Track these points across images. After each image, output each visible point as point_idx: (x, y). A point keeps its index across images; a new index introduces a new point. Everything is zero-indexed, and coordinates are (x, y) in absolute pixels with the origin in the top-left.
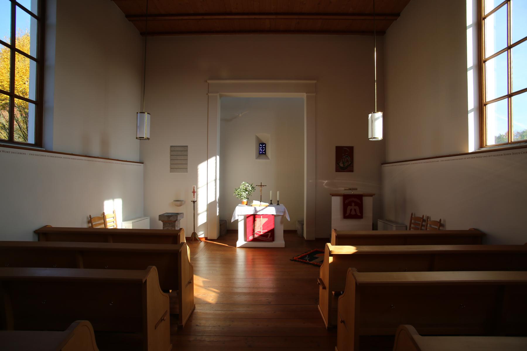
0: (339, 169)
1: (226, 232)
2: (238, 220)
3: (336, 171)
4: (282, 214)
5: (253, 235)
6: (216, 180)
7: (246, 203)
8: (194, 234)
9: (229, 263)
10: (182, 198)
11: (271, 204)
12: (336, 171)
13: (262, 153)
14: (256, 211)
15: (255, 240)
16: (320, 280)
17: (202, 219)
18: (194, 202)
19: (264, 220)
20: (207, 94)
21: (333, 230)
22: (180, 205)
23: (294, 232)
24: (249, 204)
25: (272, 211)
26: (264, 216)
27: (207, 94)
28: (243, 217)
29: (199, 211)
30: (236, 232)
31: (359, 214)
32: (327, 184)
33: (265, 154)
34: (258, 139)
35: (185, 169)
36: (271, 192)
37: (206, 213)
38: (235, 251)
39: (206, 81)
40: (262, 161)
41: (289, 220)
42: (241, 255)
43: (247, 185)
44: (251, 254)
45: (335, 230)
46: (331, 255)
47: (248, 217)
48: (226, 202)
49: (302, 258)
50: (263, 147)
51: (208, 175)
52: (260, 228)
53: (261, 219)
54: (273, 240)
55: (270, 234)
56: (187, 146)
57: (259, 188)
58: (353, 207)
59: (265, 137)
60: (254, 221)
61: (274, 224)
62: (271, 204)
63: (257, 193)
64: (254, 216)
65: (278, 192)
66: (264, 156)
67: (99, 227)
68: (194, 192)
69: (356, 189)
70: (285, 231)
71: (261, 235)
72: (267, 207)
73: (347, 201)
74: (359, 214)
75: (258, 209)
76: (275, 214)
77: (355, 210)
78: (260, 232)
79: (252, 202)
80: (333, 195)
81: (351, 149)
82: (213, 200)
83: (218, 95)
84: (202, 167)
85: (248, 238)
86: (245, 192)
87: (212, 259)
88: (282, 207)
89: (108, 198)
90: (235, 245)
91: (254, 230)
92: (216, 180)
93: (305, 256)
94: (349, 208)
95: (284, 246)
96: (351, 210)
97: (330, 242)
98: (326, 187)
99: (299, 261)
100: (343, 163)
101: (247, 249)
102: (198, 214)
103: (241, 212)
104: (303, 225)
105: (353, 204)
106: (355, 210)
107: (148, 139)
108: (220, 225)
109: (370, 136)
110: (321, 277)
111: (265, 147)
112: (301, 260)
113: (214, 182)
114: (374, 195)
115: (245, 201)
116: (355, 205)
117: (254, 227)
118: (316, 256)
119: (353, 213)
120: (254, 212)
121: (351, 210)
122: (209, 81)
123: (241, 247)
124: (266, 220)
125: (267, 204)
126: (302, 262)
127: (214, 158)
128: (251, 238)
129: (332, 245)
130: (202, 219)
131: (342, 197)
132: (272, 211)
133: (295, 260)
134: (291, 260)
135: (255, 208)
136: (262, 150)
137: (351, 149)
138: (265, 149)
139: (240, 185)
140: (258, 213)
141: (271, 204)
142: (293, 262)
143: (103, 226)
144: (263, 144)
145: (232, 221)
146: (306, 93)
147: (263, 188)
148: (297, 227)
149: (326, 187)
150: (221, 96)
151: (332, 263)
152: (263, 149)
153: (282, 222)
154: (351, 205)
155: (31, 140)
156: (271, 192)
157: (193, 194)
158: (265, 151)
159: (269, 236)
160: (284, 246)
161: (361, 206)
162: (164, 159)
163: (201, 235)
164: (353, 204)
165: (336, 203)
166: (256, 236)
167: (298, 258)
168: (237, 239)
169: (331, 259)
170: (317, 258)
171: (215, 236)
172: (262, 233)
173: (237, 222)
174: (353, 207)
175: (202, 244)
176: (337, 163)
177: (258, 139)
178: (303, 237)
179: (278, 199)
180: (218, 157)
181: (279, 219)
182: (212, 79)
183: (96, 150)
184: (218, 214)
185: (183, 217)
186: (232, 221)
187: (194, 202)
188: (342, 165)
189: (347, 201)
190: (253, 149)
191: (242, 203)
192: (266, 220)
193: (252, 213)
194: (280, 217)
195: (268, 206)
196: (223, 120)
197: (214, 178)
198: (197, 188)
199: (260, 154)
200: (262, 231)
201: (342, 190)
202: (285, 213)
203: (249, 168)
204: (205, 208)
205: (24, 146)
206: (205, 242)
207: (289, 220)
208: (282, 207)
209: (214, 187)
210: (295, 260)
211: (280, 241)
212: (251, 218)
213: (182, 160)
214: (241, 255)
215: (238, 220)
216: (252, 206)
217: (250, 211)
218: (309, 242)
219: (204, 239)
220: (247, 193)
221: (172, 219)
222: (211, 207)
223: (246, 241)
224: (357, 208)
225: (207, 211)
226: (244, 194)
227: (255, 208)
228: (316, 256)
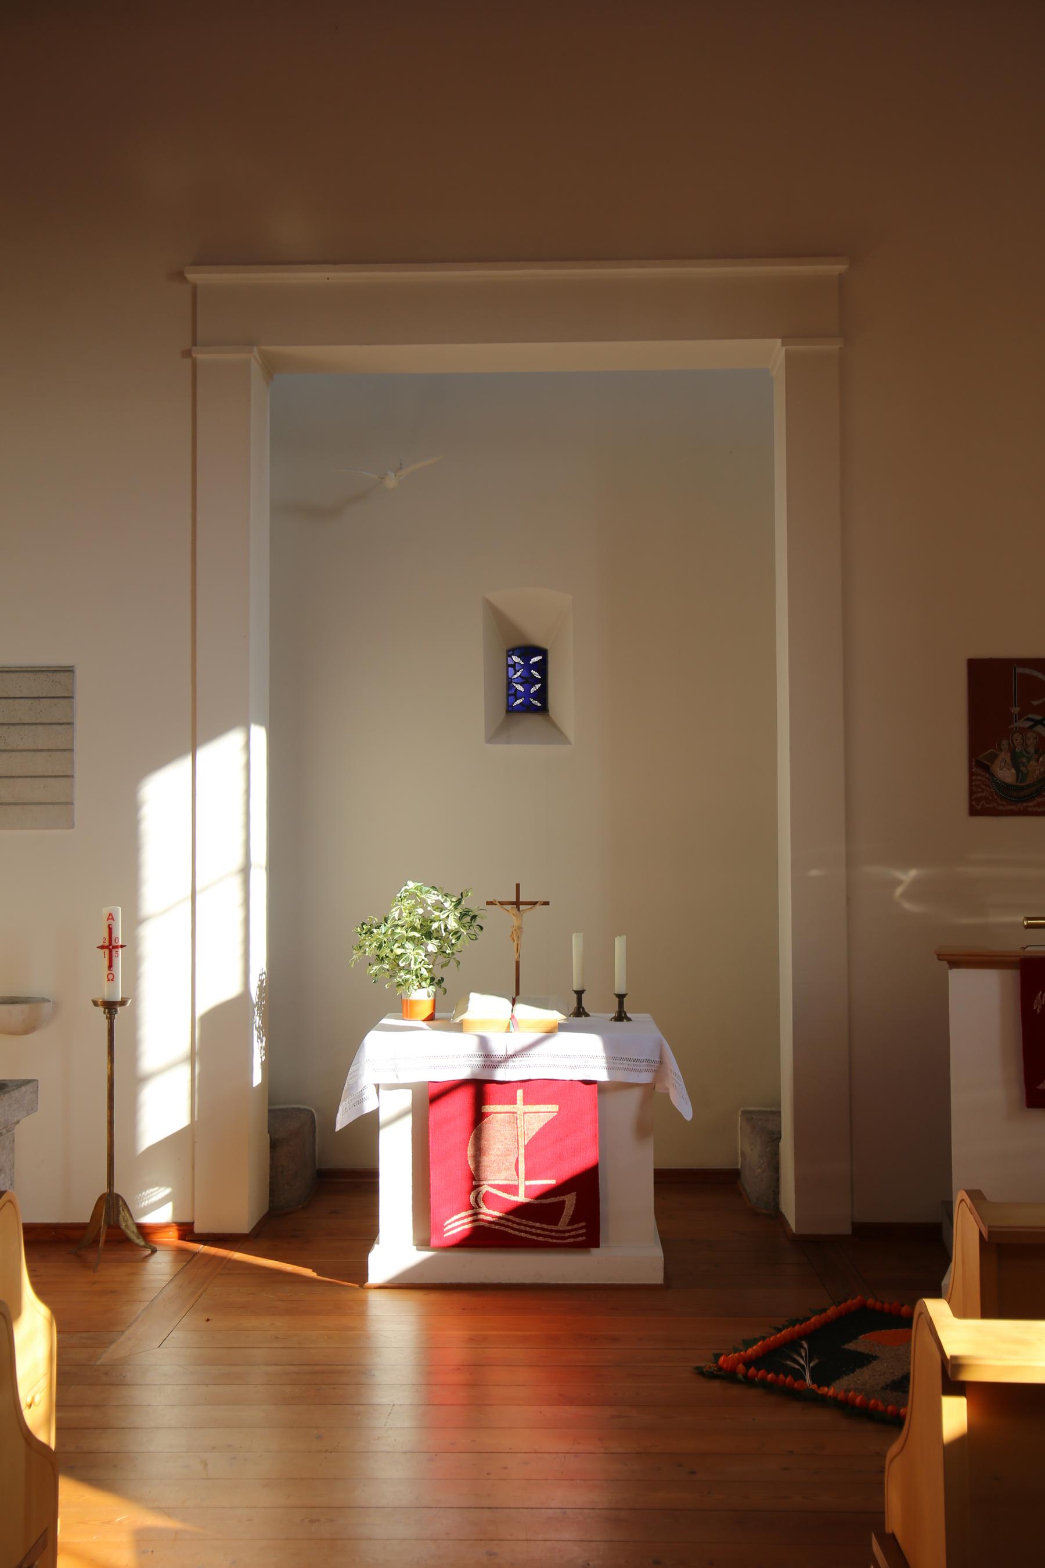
1: (311, 1187)
2: (375, 1114)
3: (973, 812)
4: (645, 1078)
5: (474, 1209)
6: (246, 871)
7: (427, 1012)
8: (111, 1204)
9: (324, 1389)
10: (37, 984)
11: (578, 1012)
12: (973, 812)
13: (527, 708)
14: (490, 1061)
15: (481, 1238)
16: (890, 1543)
17: (164, 1108)
18: (111, 1007)
19: (537, 1117)
20: (187, 353)
21: (960, 1196)
22: (28, 1029)
23: (723, 1181)
24: (444, 1015)
25: (582, 1056)
26: (538, 1090)
27: (187, 353)
28: (405, 1099)
29: (150, 1058)
30: (365, 1182)
32: (916, 891)
33: (544, 709)
34: (498, 620)
35: (60, 809)
36: (577, 942)
37: (185, 1071)
38: (360, 1311)
39: (180, 276)
40: (526, 753)
41: (687, 1112)
42: (394, 1333)
43: (432, 898)
44: (456, 1333)
45: (976, 1196)
46: (954, 1386)
47: (434, 1096)
48: (306, 1005)
49: (773, 1357)
50: (528, 667)
51: (199, 842)
52: (512, 1166)
53: (520, 1107)
54: (591, 1240)
55: (570, 1200)
56: (69, 670)
57: (508, 917)
59: (545, 610)
60: (478, 1118)
61: (600, 1137)
62: (580, 1012)
63: (494, 947)
64: (480, 1091)
65: (620, 944)
66: (533, 721)
68: (110, 947)
70: (666, 1180)
71: (520, 1211)
72: (551, 1032)
75: (500, 1047)
76: (601, 1075)
78: (512, 1189)
79: (461, 1003)
80: (958, 961)
82: (232, 990)
83: (253, 358)
84: (162, 793)
85: (440, 1229)
86: (417, 943)
87: (219, 1369)
88: (644, 1030)
90: (360, 1274)
91: (475, 1180)
92: (246, 871)
93: (792, 1345)
95: (657, 1277)
97: (937, 1294)
98: (907, 906)
99: (749, 1382)
100: (1016, 763)
101: (434, 1297)
102: (138, 1081)
103: (393, 1068)
104: (775, 1138)
108: (274, 1145)
110: (894, 1523)
112: (766, 1373)
113: (237, 881)
115: (422, 996)
117: (479, 1152)
118: (860, 1344)
120: (490, 1064)
122: (197, 277)
123: (398, 1285)
124: (547, 1111)
125: (556, 1016)
126: (764, 1385)
127: (234, 739)
128: (457, 1225)
129: (961, 1312)
130: (164, 1108)
131: (1012, 976)
132: (582, 1056)
133: (727, 1376)
134: (701, 1372)
135: (483, 1042)
136: (527, 689)
138: (544, 681)
139: (390, 900)
140: (500, 1075)
141: (580, 1012)
142: (716, 1385)
144: (527, 651)
145: (342, 1121)
146: (787, 338)
147: (530, 915)
148: (740, 1150)
149: (907, 906)
150: (271, 367)
151: (960, 1442)
152: (528, 681)
153: (643, 1129)
156: (1035, 703)
157: (102, 957)
158: (542, 695)
159: (569, 1210)
160: (657, 1277)
163: (157, 1208)
165: (979, 1009)
166: (489, 1213)
167: (748, 1363)
168: (369, 1234)
169: (955, 1415)
170: (862, 1360)
171: (240, 1211)
172: (521, 1198)
173: (368, 1126)
175: (161, 1266)
176: (979, 761)
177: (498, 620)
178: (778, 1216)
179: (620, 987)
180: (259, 735)
181: (628, 1104)
182: (201, 262)
184: (257, 1078)
185: (32, 1108)
186: (342, 1121)
187: (111, 1007)
188: (1006, 774)
190: (472, 682)
191: (402, 1008)
192: (547, 1111)
193: (463, 1073)
194: (635, 1095)
195: (561, 1027)
196: (297, 512)
197: (238, 861)
198: (135, 920)
199: (510, 710)
200: (523, 1184)
201: (1009, 925)
202: (659, 1067)
203: (447, 797)
204: (181, 1042)
206: (180, 1251)
207: (687, 1112)
208: (644, 1030)
209: (240, 915)
210: (727, 1376)
211: (632, 1247)
212: (462, 1100)
214: (394, 1333)
215: (375, 1114)
216: (459, 1027)
217: (450, 1058)
218: (813, 1246)
219: (171, 1237)
220: (432, 946)
222: (216, 1034)
223: (423, 1243)
225: (192, 1057)
226: (416, 956)
227: (483, 1042)
228: (860, 1344)
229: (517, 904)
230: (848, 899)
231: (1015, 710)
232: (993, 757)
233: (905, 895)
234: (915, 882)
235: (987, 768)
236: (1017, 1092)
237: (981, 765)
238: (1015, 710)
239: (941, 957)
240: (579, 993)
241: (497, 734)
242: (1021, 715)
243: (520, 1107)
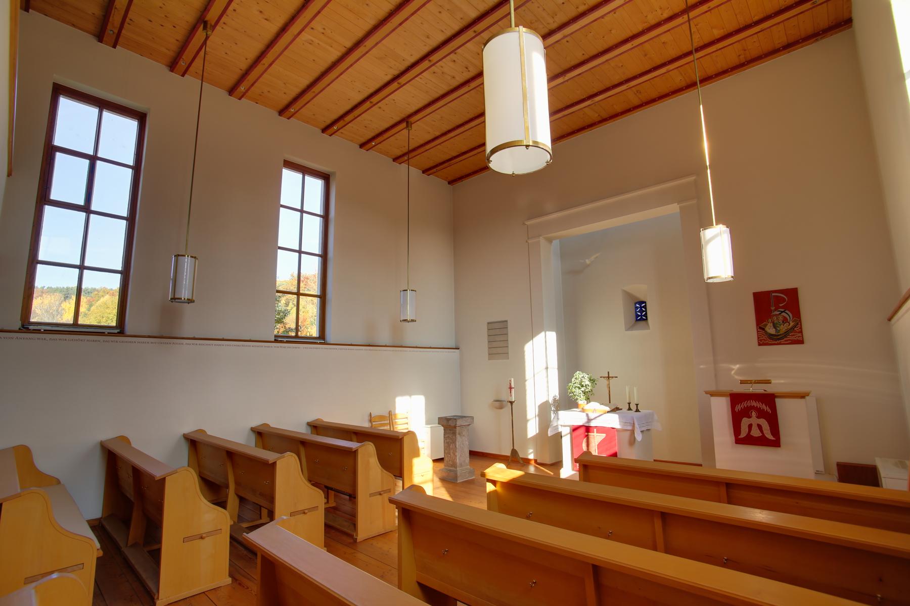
0: (766, 339)
13: (642, 319)
14: (589, 420)
26: (600, 430)
31: (770, 436)
32: (739, 372)
34: (628, 295)
35: (506, 355)
39: (524, 224)
40: (639, 333)
47: (575, 429)
53: (595, 434)
56: (506, 321)
57: (605, 381)
58: (754, 420)
59: (641, 290)
66: (642, 323)
67: (385, 428)
69: (768, 382)
73: (738, 408)
74: (770, 436)
75: (592, 416)
77: (760, 427)
81: (792, 294)
89: (402, 394)
94: (745, 422)
96: (750, 426)
98: (736, 377)
100: (775, 327)
105: (754, 414)
106: (760, 427)
107: (413, 321)
109: (706, 278)
111: (645, 307)
114: (808, 394)
116: (758, 417)
119: (756, 433)
121: (750, 426)
122: (528, 223)
131: (729, 399)
132: (613, 421)
135: (587, 415)
137: (792, 294)
140: (593, 424)
143: (387, 428)
149: (736, 377)
152: (641, 311)
154: (749, 417)
155: (314, 331)
158: (646, 315)
161: (773, 419)
162: (480, 342)
164: (754, 414)
165: (721, 409)
174: (754, 420)
176: (760, 327)
177: (628, 295)
182: (530, 218)
183: (384, 337)
188: (770, 330)
189: (738, 408)
199: (637, 320)
205: (308, 340)
213: (502, 341)
221: (451, 423)
224: (764, 423)
225: (539, 415)
229: (609, 377)
230: (716, 375)
231: (773, 308)
232: (766, 325)
233: (736, 373)
234: (739, 369)
235: (763, 329)
236: (732, 438)
237: (760, 328)
238: (773, 308)
239: (707, 393)
240: (629, 404)
241: (630, 328)
242: (775, 310)
243: (595, 434)
